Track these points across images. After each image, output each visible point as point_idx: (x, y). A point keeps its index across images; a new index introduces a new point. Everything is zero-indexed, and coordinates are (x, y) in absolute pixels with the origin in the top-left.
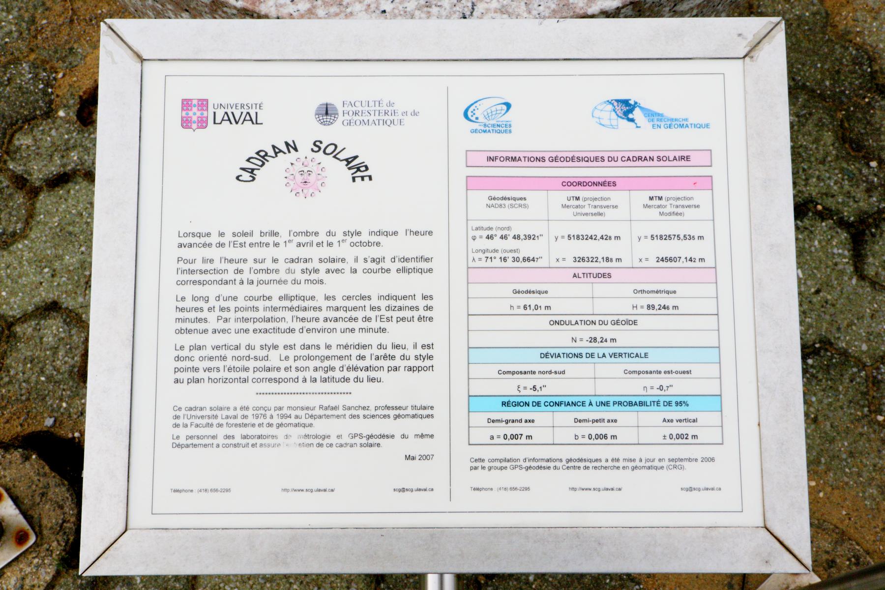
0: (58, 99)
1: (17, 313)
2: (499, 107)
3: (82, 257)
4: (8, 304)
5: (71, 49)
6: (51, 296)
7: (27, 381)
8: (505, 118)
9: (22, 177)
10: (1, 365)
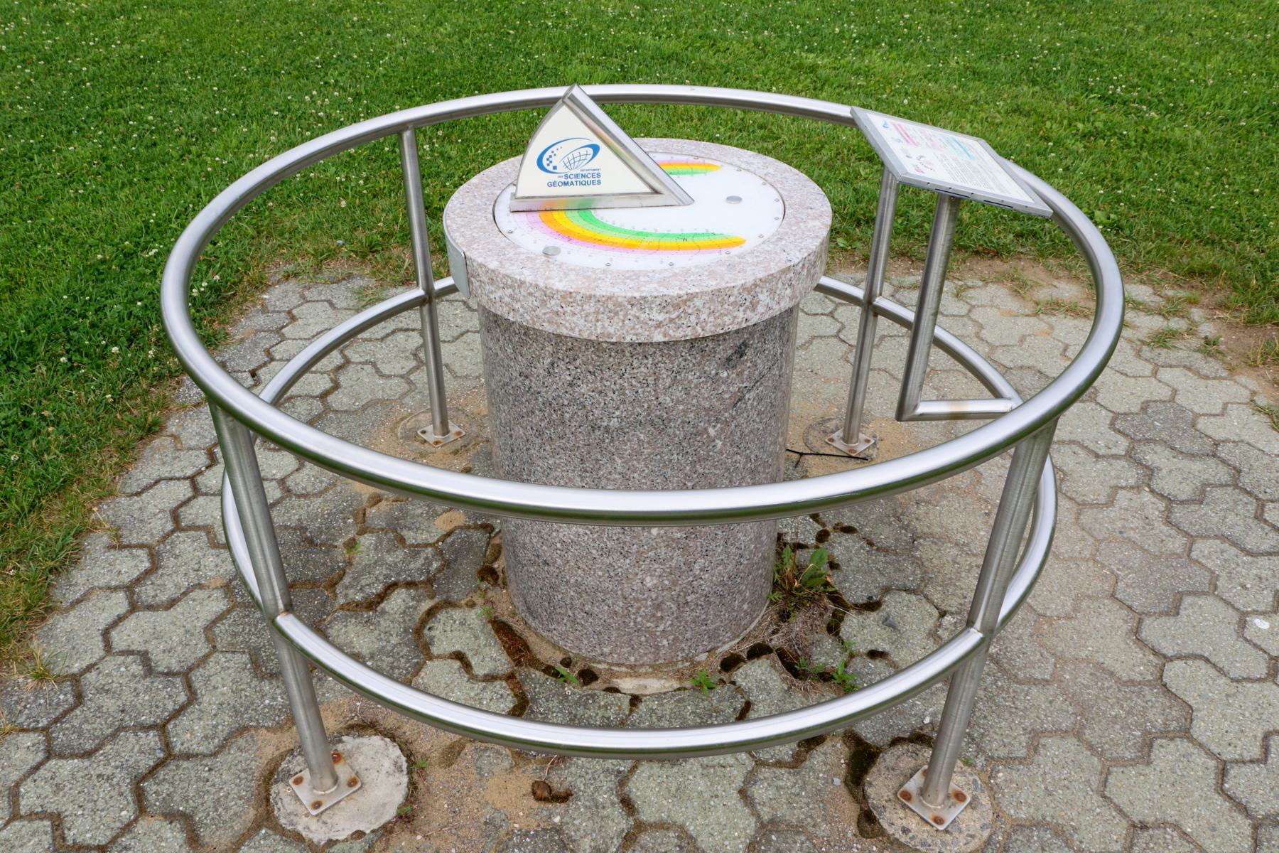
0: (542, 825)
1: (753, 820)
2: (583, 151)
3: (698, 777)
4: (745, 829)
5: (486, 823)
6: (735, 795)
7: (808, 804)
8: (590, 166)
9: (625, 838)
10: (797, 849)
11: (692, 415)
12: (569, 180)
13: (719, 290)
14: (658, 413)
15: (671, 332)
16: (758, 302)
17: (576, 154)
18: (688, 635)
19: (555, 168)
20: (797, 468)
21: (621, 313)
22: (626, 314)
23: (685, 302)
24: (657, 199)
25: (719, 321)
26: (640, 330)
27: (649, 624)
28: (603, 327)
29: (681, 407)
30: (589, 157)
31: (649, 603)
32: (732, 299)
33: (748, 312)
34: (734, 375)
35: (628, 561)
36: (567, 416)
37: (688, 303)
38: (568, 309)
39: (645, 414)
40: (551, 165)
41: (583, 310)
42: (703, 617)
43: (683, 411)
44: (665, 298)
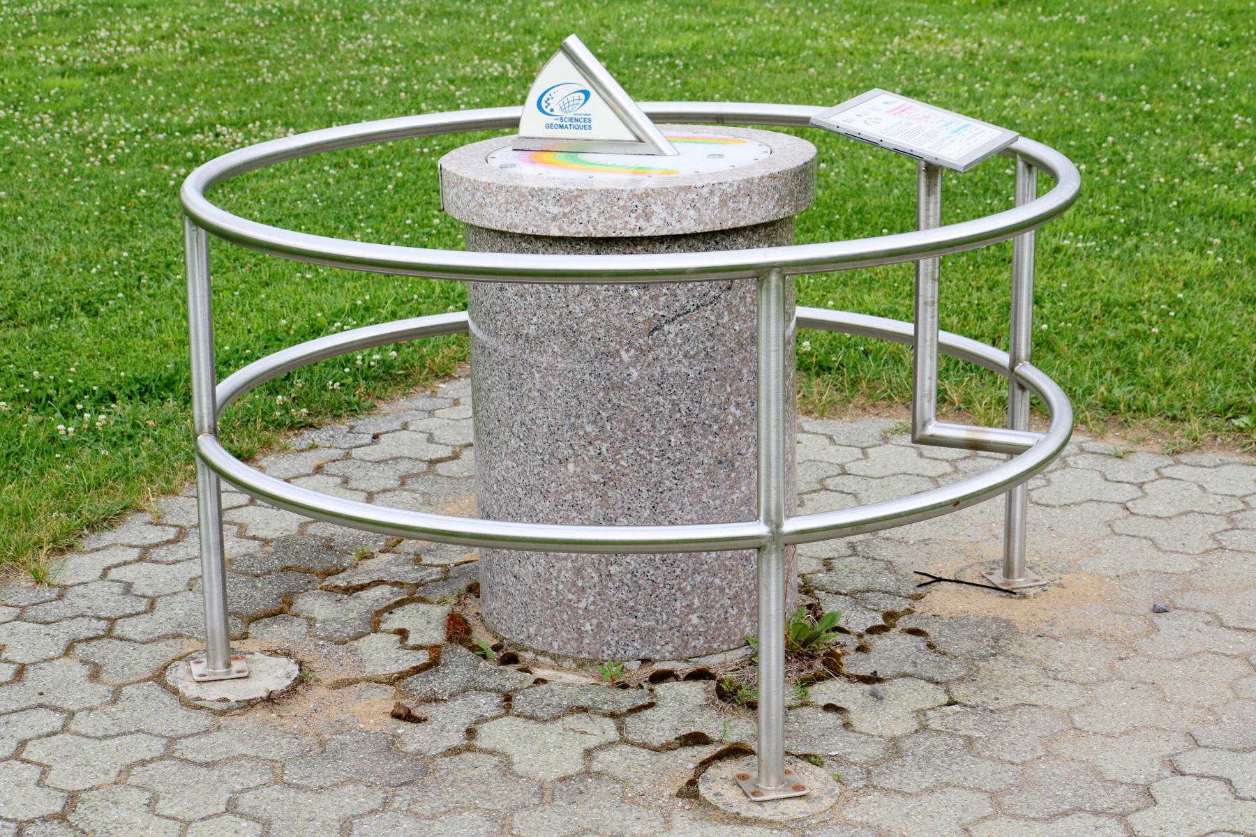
2: (576, 96)
11: (602, 331)
12: (564, 123)
13: (607, 191)
14: (569, 323)
15: (565, 227)
16: (652, 213)
17: (570, 98)
18: (614, 624)
19: (552, 110)
20: (356, 109)
21: (524, 204)
22: (527, 206)
23: (576, 197)
24: (641, 148)
25: (610, 223)
26: (539, 222)
27: (570, 596)
28: (512, 218)
29: (591, 320)
30: (581, 102)
31: (570, 565)
32: (621, 203)
33: (641, 220)
34: (647, 298)
35: (548, 504)
36: (499, 324)
37: (579, 199)
38: (488, 200)
39: (557, 322)
40: (549, 107)
41: (497, 200)
42: (631, 603)
43: (593, 324)
44: (559, 192)
